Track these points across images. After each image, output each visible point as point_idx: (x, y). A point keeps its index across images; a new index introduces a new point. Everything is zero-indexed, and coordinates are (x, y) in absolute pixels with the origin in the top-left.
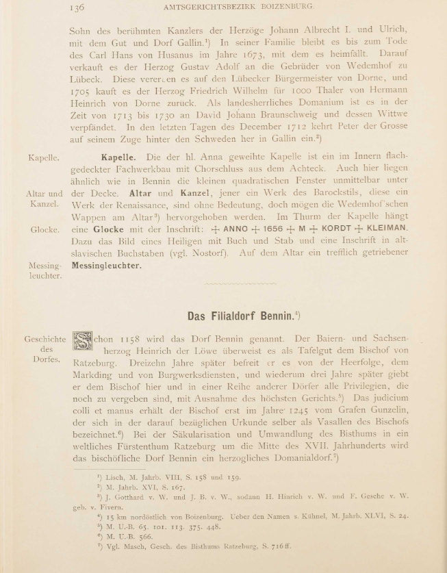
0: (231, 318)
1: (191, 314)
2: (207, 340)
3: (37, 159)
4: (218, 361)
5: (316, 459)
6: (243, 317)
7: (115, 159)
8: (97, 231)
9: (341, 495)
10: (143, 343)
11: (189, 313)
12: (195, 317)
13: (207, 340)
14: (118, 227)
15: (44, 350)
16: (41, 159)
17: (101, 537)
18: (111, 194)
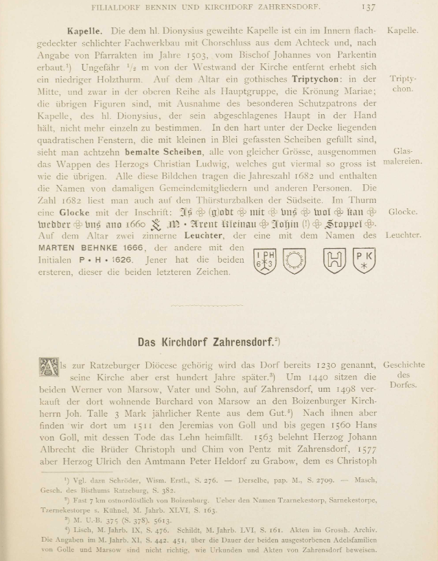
0: (225, 344)
1: (141, 340)
2: (276, 366)
3: (77, 32)
4: (182, 388)
5: (232, 462)
6: (196, 343)
7: (81, 32)
8: (63, 214)
9: (277, 483)
10: (179, 370)
11: (139, 339)
12: (145, 343)
13: (276, 366)
14: (84, 211)
15: (402, 375)
16: (399, 32)
17: (67, 501)
18: (327, 128)
